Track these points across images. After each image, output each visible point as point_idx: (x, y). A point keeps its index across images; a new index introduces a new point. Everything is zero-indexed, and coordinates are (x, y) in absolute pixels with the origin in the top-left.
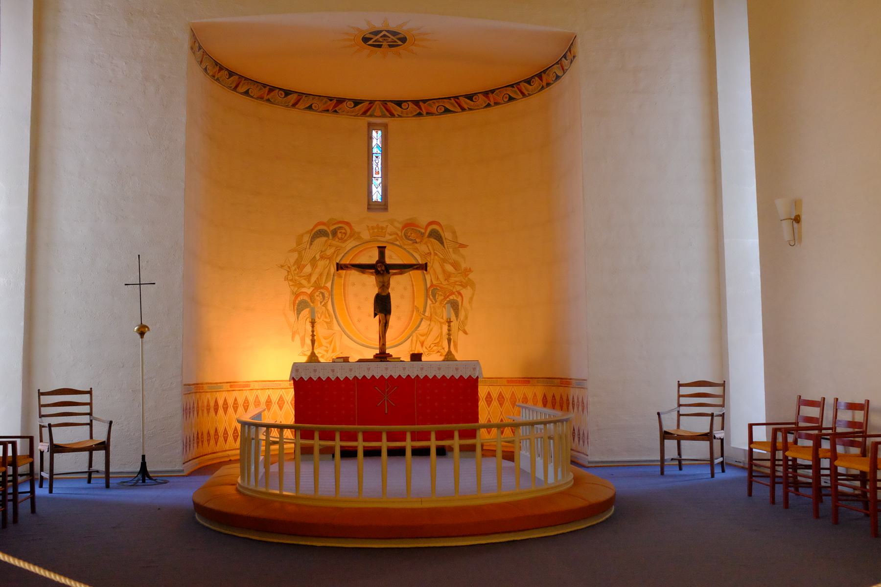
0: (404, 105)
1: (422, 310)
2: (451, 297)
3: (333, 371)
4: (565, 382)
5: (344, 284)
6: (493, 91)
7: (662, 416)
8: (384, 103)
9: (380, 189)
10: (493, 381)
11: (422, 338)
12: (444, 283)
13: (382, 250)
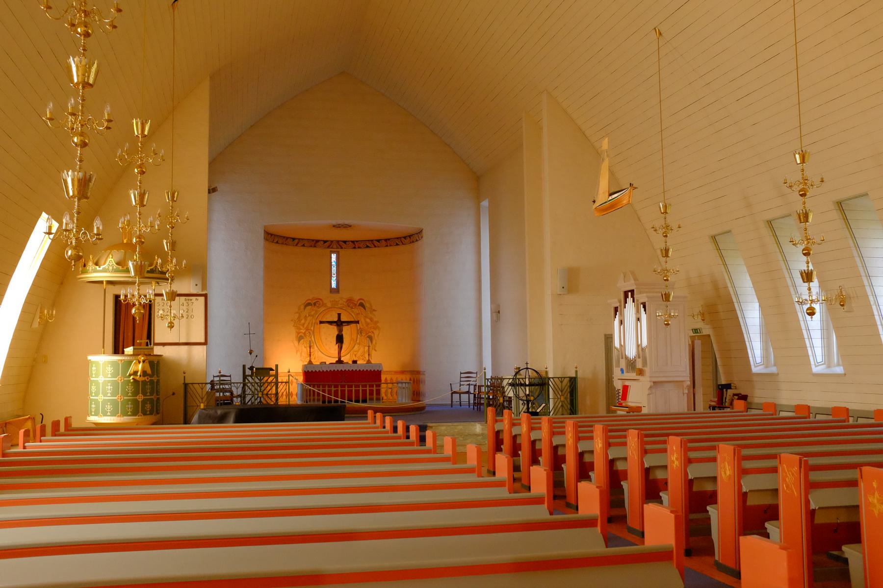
0: (347, 243)
1: (355, 340)
2: (369, 334)
3: (321, 368)
4: (418, 373)
5: (319, 328)
6: (389, 239)
7: (452, 385)
8: (338, 242)
9: (335, 282)
10: (388, 372)
11: (355, 353)
12: (367, 327)
13: (339, 315)
